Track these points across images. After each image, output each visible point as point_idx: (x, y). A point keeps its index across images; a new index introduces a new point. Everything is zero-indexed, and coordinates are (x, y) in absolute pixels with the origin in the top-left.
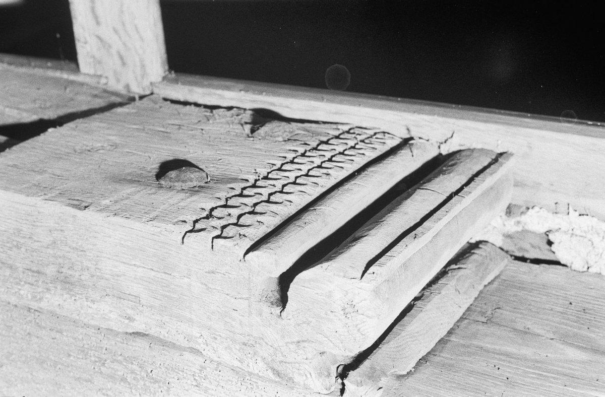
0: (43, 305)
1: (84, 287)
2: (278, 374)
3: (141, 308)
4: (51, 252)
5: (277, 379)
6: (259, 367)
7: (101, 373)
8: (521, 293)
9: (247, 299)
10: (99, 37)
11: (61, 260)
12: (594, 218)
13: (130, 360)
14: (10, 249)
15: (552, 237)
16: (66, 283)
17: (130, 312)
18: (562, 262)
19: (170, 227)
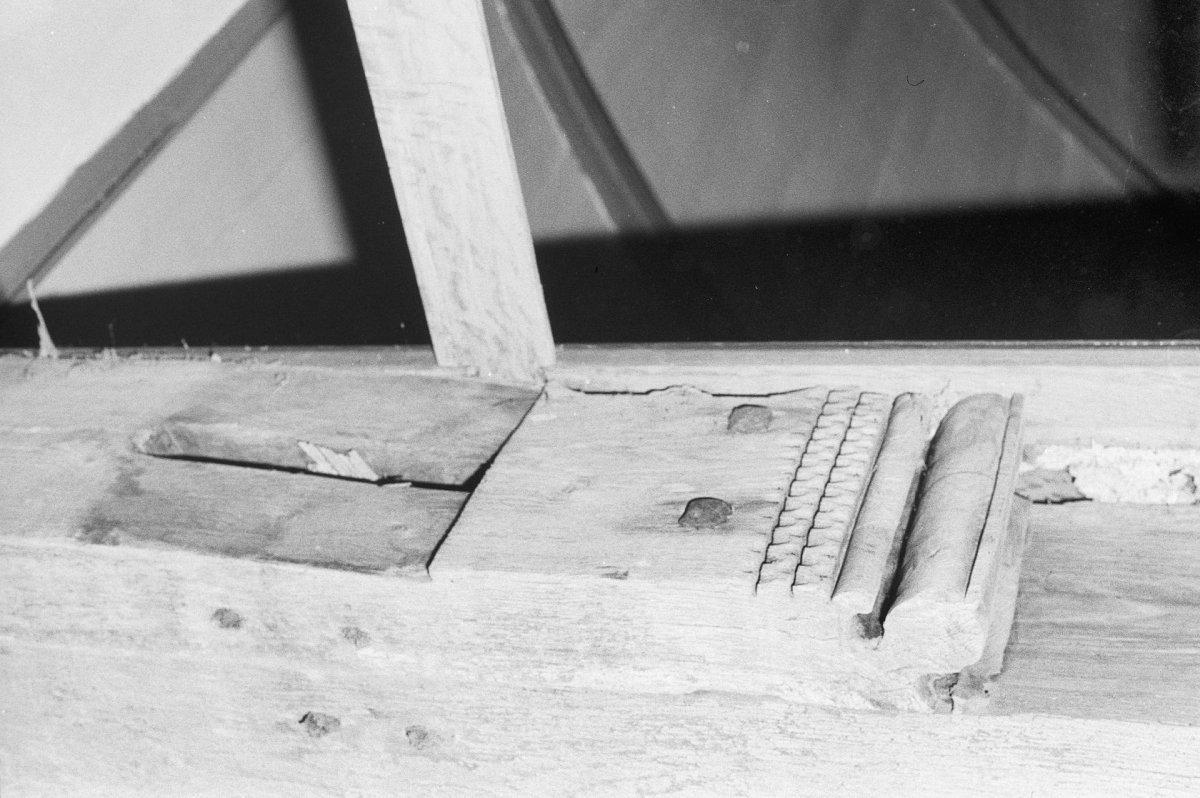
0: (575, 684)
1: (630, 656)
2: (878, 704)
3: (706, 667)
4: (584, 627)
5: (878, 709)
6: (856, 701)
7: (656, 741)
8: (1062, 547)
9: (836, 638)
10: (465, 324)
11: (598, 634)
12: (1110, 449)
13: (692, 721)
14: (525, 631)
15: (1073, 472)
16: (607, 657)
17: (691, 672)
18: (1088, 496)
19: (736, 581)
